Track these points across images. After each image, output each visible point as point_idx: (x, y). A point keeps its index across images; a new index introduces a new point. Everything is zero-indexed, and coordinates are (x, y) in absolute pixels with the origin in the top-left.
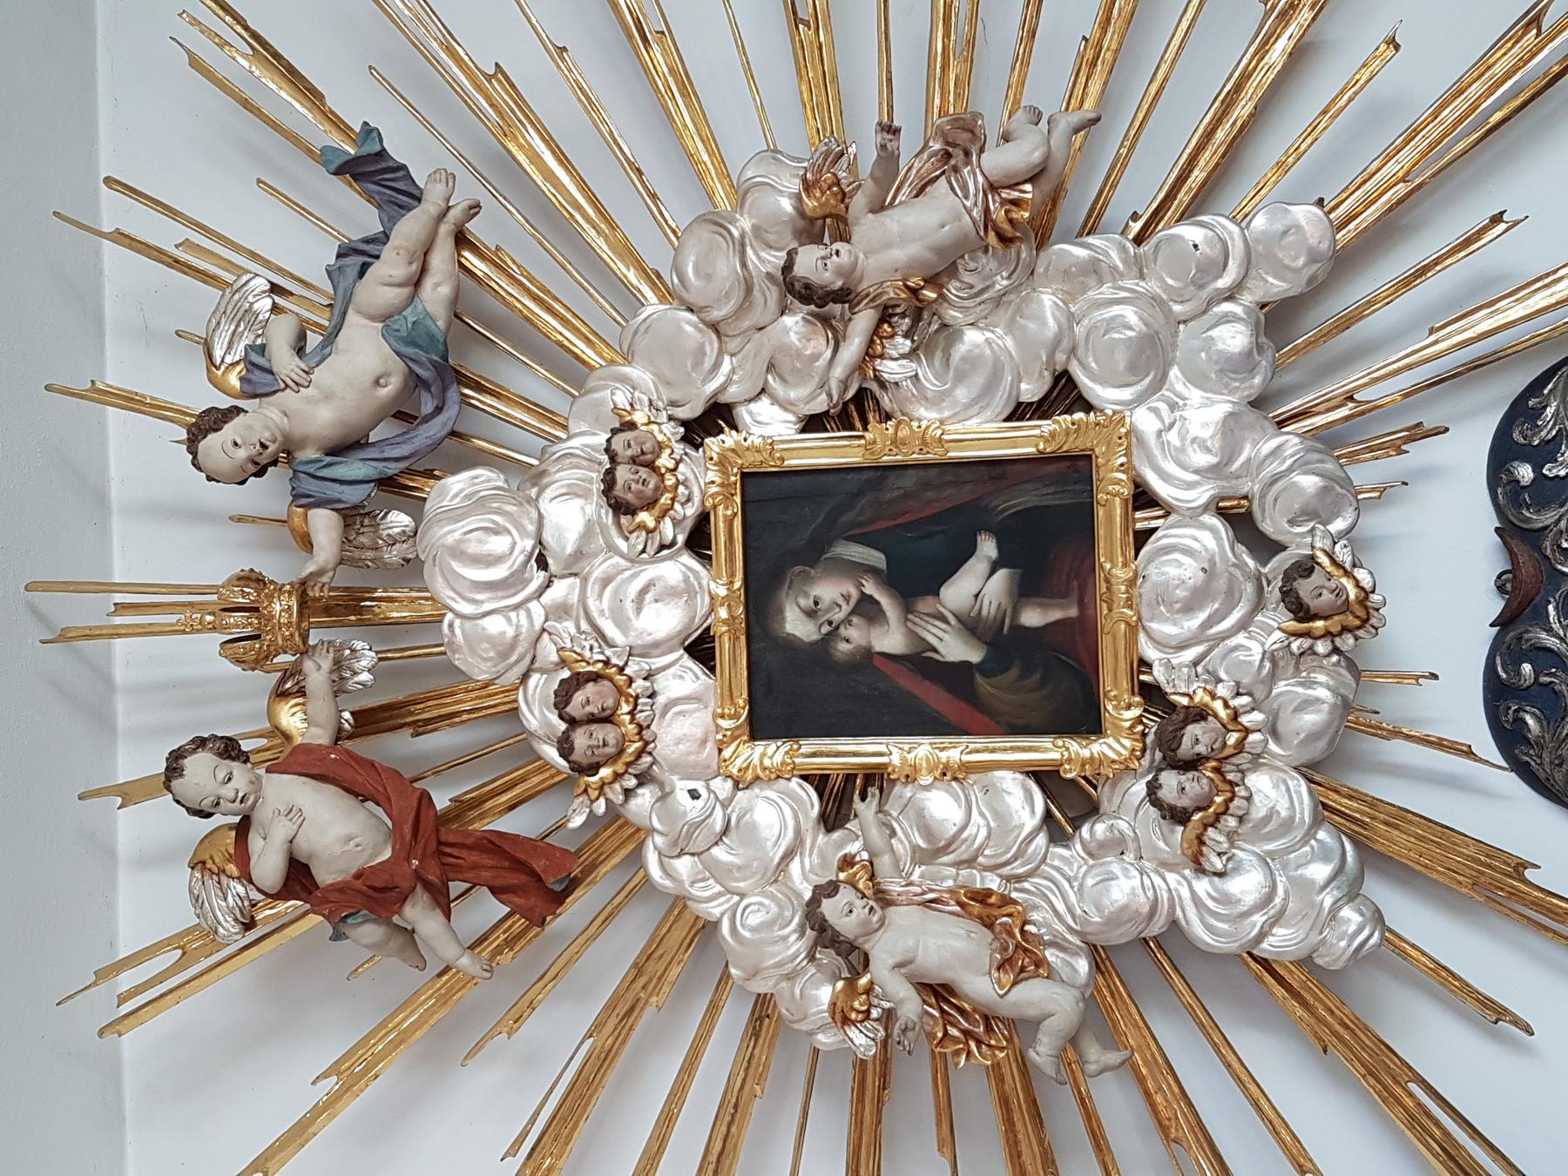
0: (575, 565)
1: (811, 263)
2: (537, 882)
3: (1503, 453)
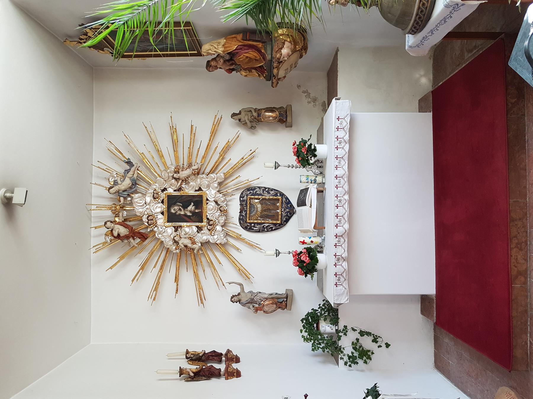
0: (149, 204)
1: (175, 176)
2: (143, 237)
3: (241, 197)
